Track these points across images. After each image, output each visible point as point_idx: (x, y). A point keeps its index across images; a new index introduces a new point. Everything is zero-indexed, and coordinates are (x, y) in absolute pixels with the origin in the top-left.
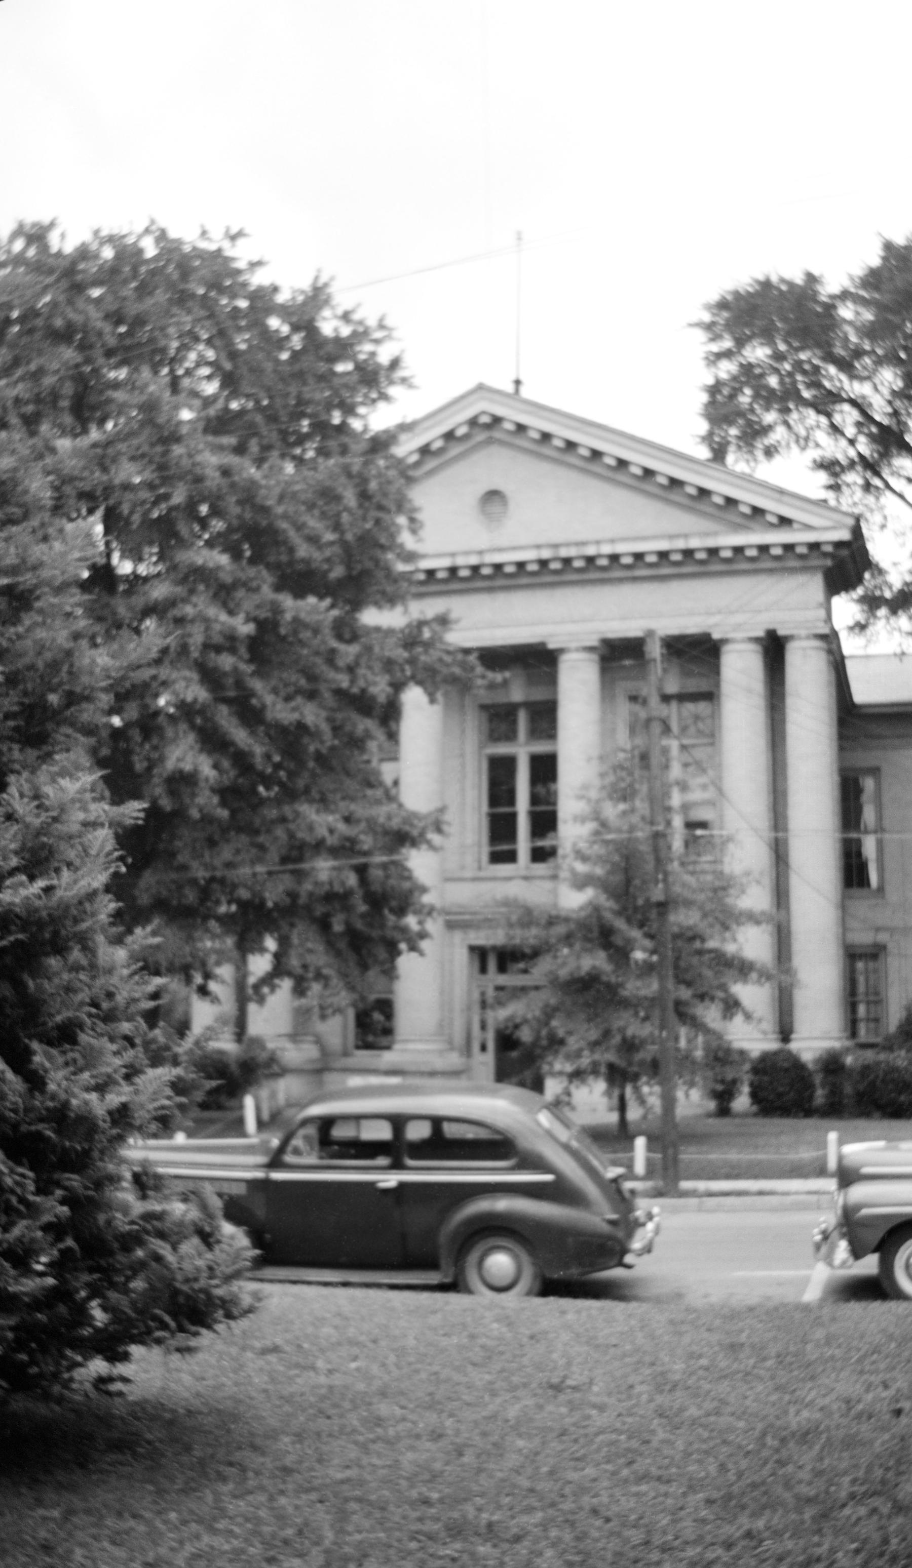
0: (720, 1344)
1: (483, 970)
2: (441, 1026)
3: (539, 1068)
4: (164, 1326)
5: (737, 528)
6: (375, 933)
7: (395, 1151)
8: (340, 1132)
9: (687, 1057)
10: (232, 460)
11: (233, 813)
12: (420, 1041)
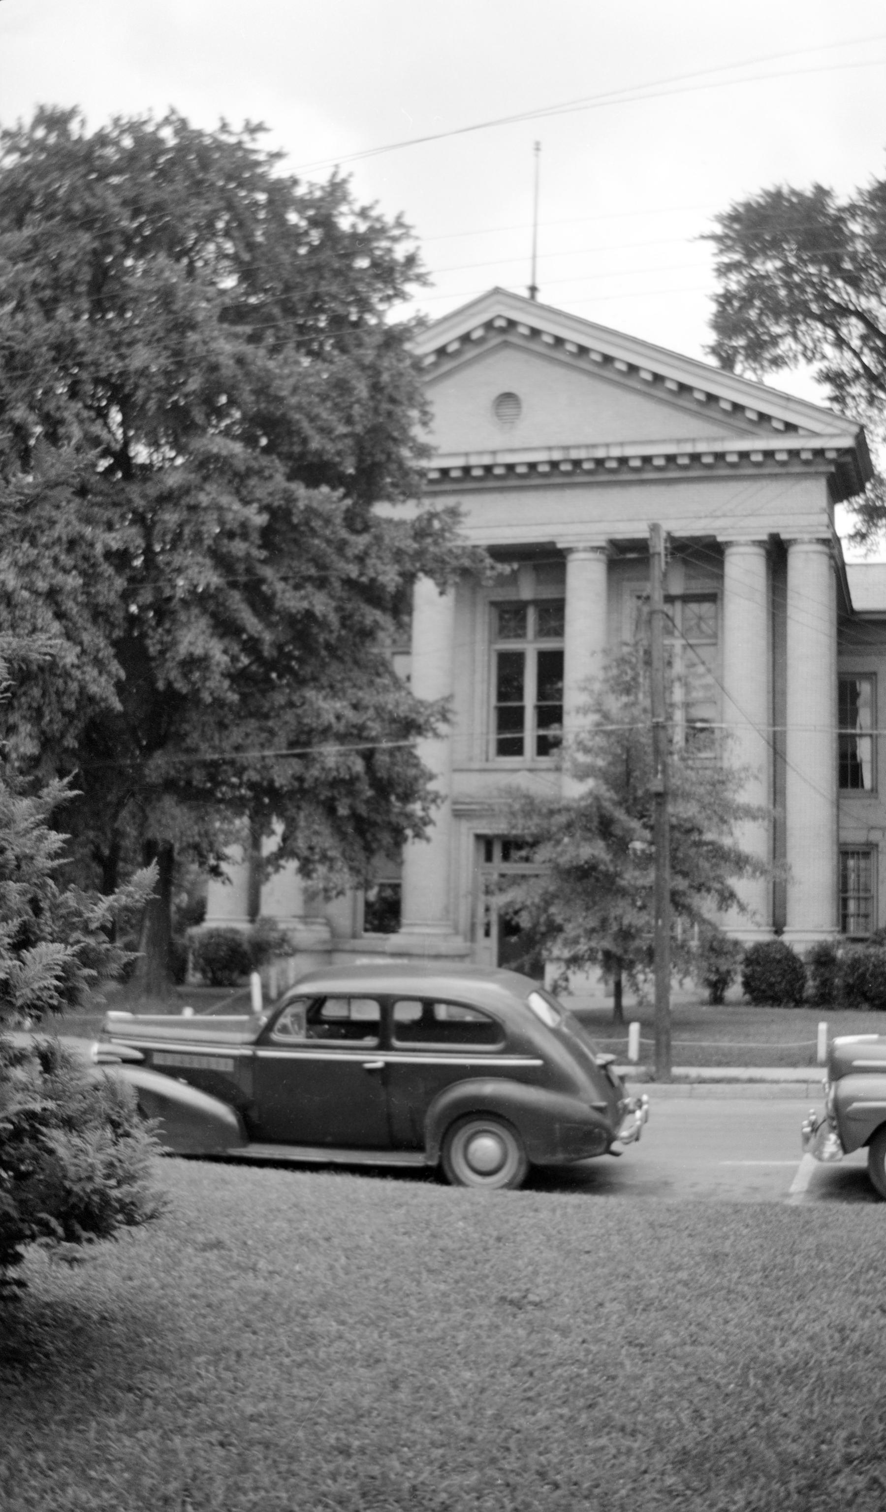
0: (702, 1253)
1: (489, 858)
2: (447, 910)
3: (539, 954)
4: (51, 1232)
5: (743, 433)
6: (379, 819)
7: (382, 1031)
8: (331, 1010)
10: (248, 349)
11: (244, 697)
12: (427, 925)
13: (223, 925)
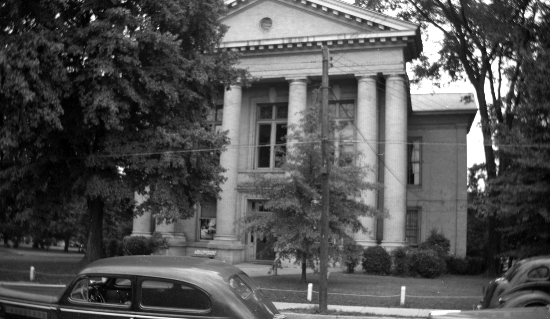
5: (365, 31)
9: (336, 248)
13: (139, 235)
